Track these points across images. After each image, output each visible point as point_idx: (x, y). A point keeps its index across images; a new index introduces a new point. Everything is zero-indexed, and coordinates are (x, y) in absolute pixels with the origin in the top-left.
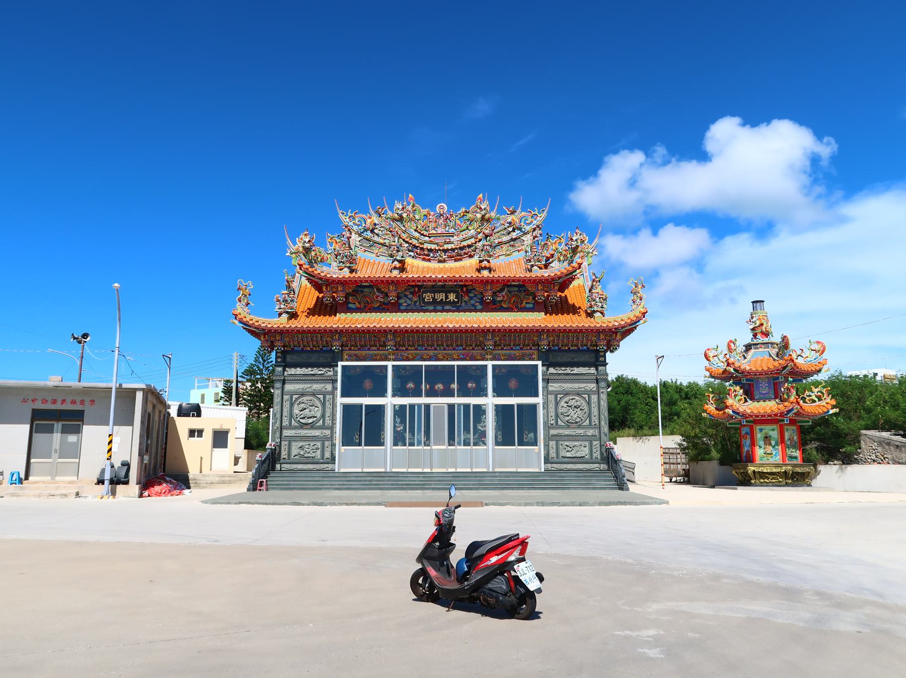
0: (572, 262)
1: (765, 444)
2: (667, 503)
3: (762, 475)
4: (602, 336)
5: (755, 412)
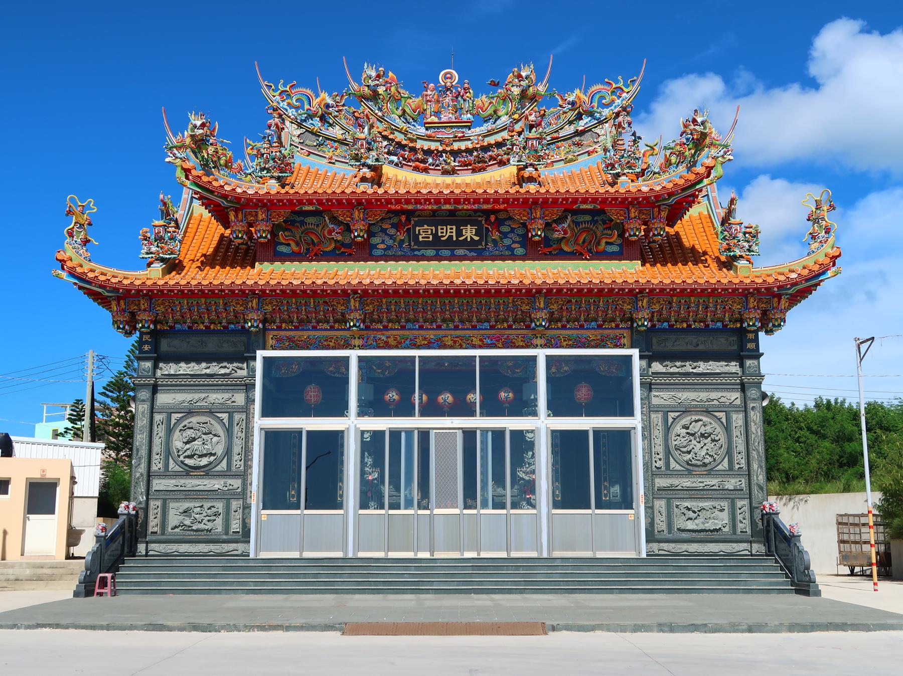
0: (694, 164)
4: (752, 303)
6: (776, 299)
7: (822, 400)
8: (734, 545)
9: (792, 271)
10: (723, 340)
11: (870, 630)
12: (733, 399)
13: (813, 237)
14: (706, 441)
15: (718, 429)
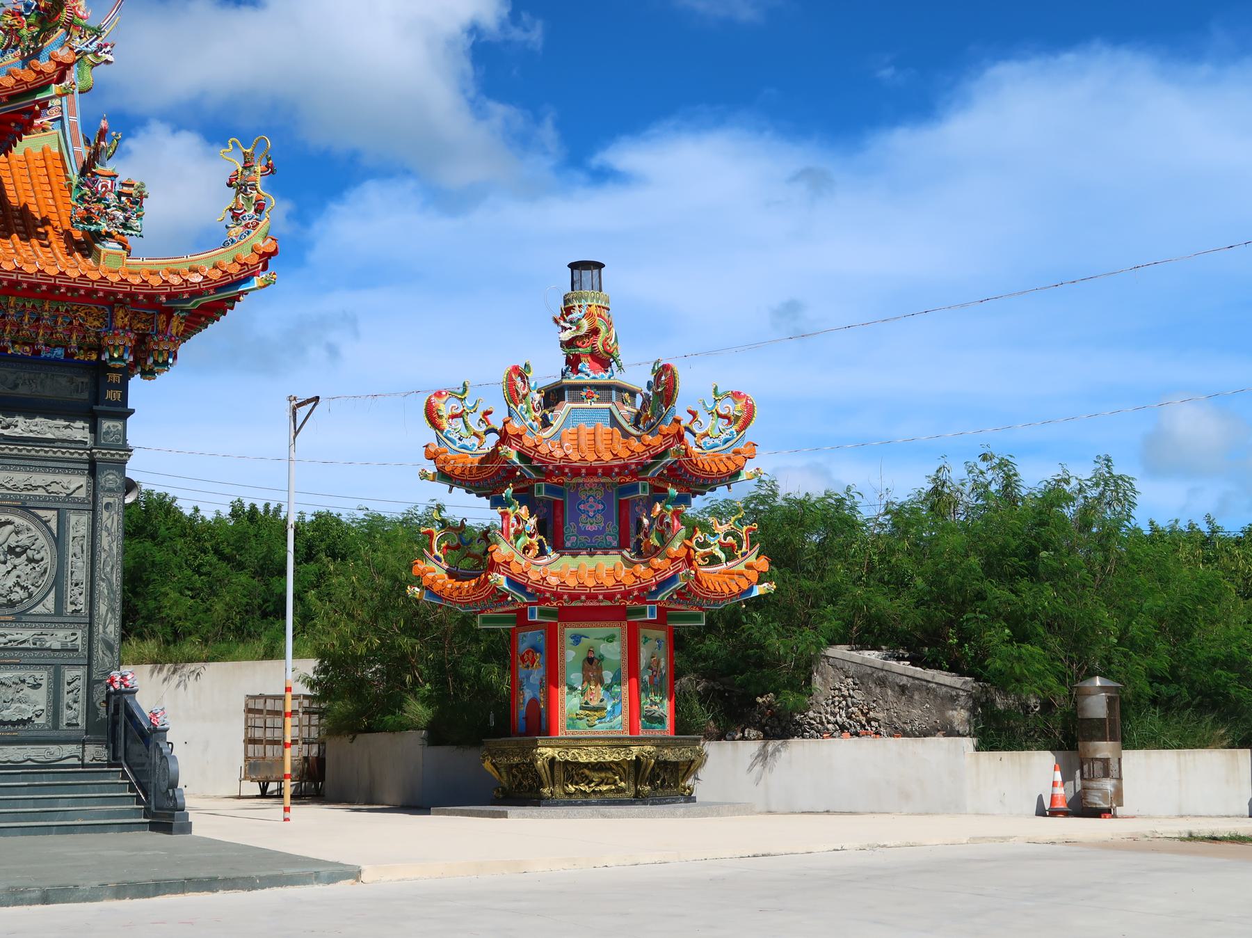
0: (37, 53)
1: (587, 679)
2: (354, 874)
3: (574, 771)
4: (121, 319)
5: (572, 583)
6: (163, 317)
7: (242, 505)
8: (53, 748)
9: (193, 270)
10: (63, 381)
11: (254, 888)
12: (73, 487)
13: (236, 217)
14: (17, 561)
15: (42, 541)
